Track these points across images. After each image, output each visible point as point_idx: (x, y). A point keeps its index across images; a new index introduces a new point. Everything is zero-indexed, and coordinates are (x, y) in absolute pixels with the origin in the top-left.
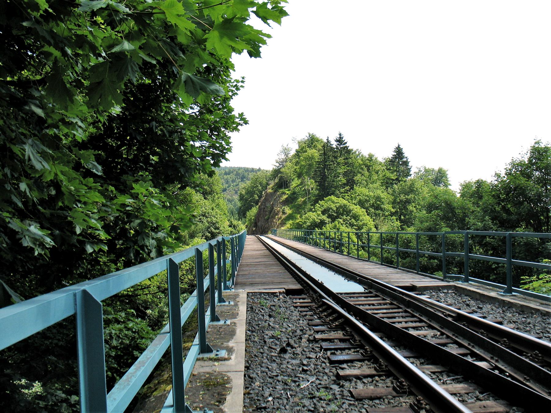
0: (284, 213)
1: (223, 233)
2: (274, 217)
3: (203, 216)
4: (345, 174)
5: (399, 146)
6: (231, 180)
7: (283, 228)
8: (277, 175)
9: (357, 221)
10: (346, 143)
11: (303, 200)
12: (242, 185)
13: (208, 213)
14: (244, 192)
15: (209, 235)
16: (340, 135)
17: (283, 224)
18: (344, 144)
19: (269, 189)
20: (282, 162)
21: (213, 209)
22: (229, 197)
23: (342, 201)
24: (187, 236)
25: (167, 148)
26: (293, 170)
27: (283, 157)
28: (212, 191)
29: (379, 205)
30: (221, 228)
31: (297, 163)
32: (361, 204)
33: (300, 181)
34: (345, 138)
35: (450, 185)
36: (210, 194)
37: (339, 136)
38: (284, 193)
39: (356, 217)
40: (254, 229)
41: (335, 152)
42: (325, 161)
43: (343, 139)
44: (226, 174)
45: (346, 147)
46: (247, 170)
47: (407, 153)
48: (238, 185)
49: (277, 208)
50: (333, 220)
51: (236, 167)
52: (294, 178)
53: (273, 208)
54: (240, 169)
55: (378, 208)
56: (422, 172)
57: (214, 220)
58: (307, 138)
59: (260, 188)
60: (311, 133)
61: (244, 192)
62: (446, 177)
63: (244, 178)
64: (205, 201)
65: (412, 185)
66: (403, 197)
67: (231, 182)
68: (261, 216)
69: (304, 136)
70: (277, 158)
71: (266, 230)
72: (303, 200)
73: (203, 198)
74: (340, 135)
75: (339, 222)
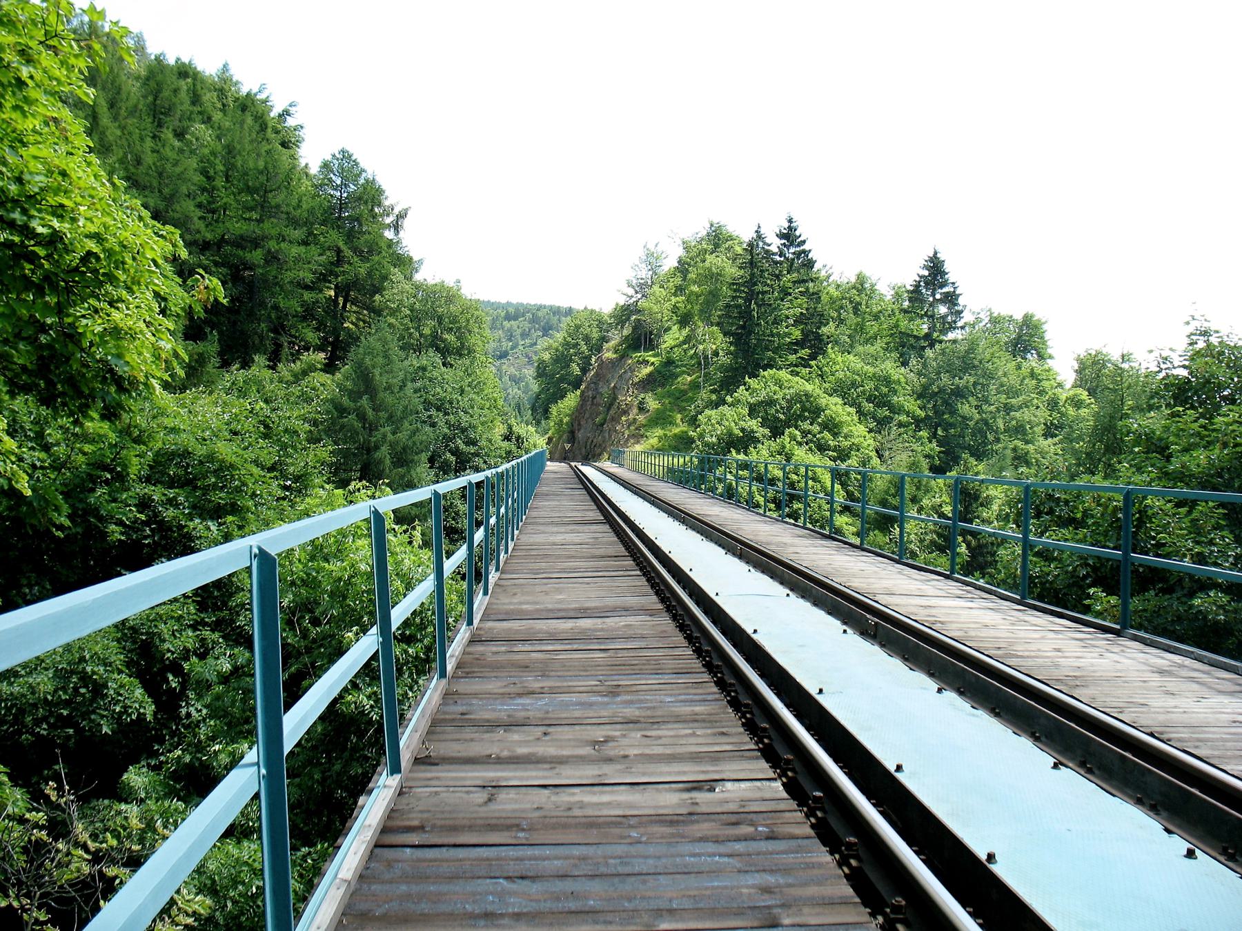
0: (642, 409)
2: (616, 420)
3: (438, 409)
5: (936, 253)
6: (519, 331)
7: (638, 448)
8: (628, 319)
9: (835, 435)
10: (804, 242)
11: (689, 379)
12: (543, 343)
13: (451, 403)
14: (546, 356)
15: (453, 459)
16: (790, 221)
17: (638, 437)
18: (799, 245)
19: (608, 350)
21: (462, 392)
22: (512, 370)
23: (800, 384)
24: (388, 462)
27: (645, 273)
30: (483, 443)
31: (679, 290)
32: (842, 390)
33: (686, 332)
34: (802, 231)
35: (1051, 357)
37: (786, 225)
38: (646, 362)
39: (832, 427)
40: (568, 446)
41: (776, 263)
42: (751, 282)
43: (797, 233)
44: (508, 317)
45: (804, 252)
46: (556, 311)
47: (954, 272)
48: (535, 344)
49: (627, 398)
50: (776, 432)
51: (533, 303)
53: (615, 398)
54: (540, 308)
55: (880, 401)
56: (984, 323)
57: (465, 419)
59: (584, 348)
60: (715, 221)
61: (546, 356)
62: (1042, 338)
63: (551, 328)
65: (972, 346)
66: (945, 379)
68: (587, 415)
69: (697, 229)
70: (630, 275)
71: (598, 451)
72: (689, 379)
74: (790, 221)
75: (793, 438)
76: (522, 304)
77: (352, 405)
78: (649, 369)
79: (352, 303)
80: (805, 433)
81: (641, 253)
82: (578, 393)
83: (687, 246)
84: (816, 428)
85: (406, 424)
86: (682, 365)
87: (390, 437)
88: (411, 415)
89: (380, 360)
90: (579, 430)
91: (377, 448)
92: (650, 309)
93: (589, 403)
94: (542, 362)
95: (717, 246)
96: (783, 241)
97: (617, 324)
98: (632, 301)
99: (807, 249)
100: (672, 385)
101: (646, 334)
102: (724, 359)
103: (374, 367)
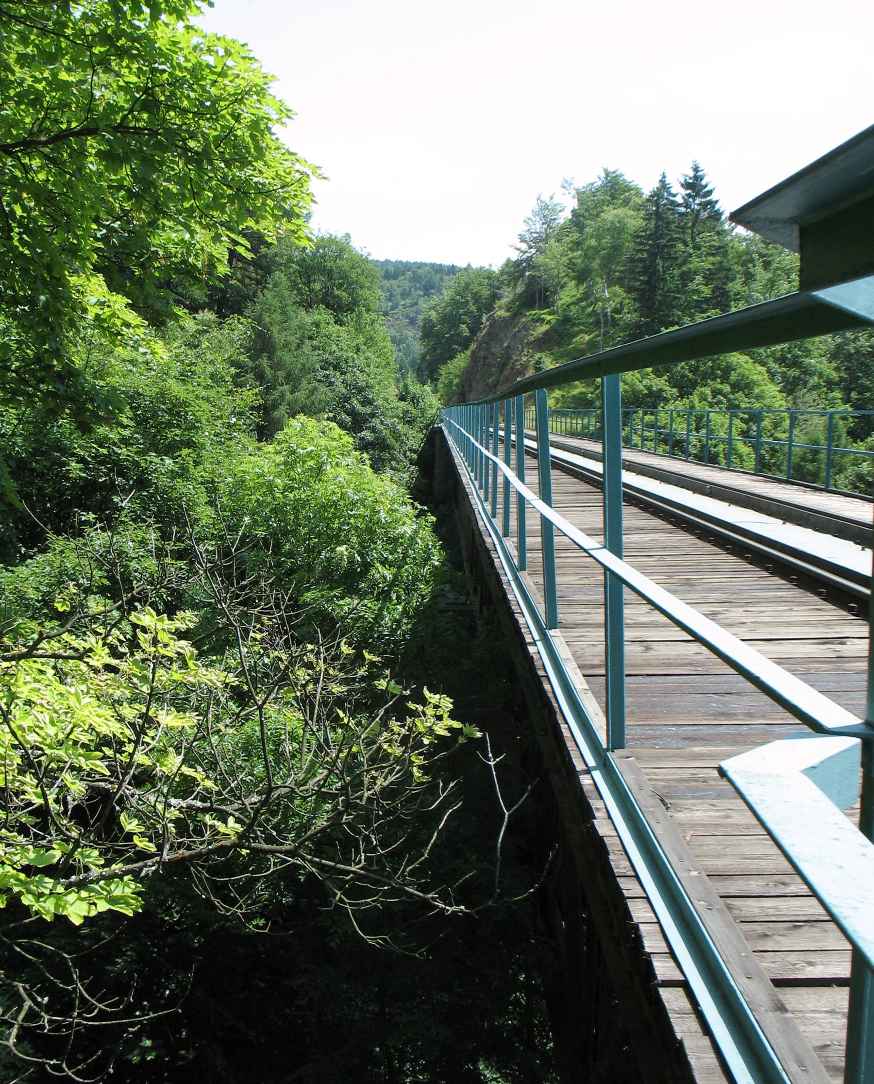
1: (383, 414)
3: (336, 367)
4: (709, 277)
10: (710, 192)
11: (587, 338)
12: (423, 305)
13: (347, 362)
14: (433, 315)
16: (696, 169)
19: (500, 308)
20: (536, 240)
21: (358, 350)
26: (565, 259)
27: (538, 227)
29: (796, 357)
30: (380, 402)
34: (710, 180)
37: (692, 174)
42: (656, 235)
43: (704, 183)
44: (388, 276)
46: (438, 269)
51: (412, 262)
52: (565, 283)
54: (420, 265)
57: (361, 379)
58: (599, 183)
59: (473, 308)
60: (611, 170)
63: (432, 287)
67: (399, 297)
68: (478, 377)
70: (522, 229)
72: (587, 338)
73: (332, 321)
74: (696, 169)
75: (703, 398)
76: (401, 262)
77: (251, 364)
78: (545, 328)
79: (238, 260)
80: (716, 393)
81: (534, 205)
82: (468, 353)
83: (581, 196)
84: (727, 388)
85: (304, 382)
88: (309, 373)
89: (277, 317)
90: (470, 392)
91: (275, 406)
92: (546, 264)
94: (428, 321)
95: (613, 197)
96: (688, 192)
97: (510, 281)
98: (525, 257)
99: (714, 199)
102: (629, 317)
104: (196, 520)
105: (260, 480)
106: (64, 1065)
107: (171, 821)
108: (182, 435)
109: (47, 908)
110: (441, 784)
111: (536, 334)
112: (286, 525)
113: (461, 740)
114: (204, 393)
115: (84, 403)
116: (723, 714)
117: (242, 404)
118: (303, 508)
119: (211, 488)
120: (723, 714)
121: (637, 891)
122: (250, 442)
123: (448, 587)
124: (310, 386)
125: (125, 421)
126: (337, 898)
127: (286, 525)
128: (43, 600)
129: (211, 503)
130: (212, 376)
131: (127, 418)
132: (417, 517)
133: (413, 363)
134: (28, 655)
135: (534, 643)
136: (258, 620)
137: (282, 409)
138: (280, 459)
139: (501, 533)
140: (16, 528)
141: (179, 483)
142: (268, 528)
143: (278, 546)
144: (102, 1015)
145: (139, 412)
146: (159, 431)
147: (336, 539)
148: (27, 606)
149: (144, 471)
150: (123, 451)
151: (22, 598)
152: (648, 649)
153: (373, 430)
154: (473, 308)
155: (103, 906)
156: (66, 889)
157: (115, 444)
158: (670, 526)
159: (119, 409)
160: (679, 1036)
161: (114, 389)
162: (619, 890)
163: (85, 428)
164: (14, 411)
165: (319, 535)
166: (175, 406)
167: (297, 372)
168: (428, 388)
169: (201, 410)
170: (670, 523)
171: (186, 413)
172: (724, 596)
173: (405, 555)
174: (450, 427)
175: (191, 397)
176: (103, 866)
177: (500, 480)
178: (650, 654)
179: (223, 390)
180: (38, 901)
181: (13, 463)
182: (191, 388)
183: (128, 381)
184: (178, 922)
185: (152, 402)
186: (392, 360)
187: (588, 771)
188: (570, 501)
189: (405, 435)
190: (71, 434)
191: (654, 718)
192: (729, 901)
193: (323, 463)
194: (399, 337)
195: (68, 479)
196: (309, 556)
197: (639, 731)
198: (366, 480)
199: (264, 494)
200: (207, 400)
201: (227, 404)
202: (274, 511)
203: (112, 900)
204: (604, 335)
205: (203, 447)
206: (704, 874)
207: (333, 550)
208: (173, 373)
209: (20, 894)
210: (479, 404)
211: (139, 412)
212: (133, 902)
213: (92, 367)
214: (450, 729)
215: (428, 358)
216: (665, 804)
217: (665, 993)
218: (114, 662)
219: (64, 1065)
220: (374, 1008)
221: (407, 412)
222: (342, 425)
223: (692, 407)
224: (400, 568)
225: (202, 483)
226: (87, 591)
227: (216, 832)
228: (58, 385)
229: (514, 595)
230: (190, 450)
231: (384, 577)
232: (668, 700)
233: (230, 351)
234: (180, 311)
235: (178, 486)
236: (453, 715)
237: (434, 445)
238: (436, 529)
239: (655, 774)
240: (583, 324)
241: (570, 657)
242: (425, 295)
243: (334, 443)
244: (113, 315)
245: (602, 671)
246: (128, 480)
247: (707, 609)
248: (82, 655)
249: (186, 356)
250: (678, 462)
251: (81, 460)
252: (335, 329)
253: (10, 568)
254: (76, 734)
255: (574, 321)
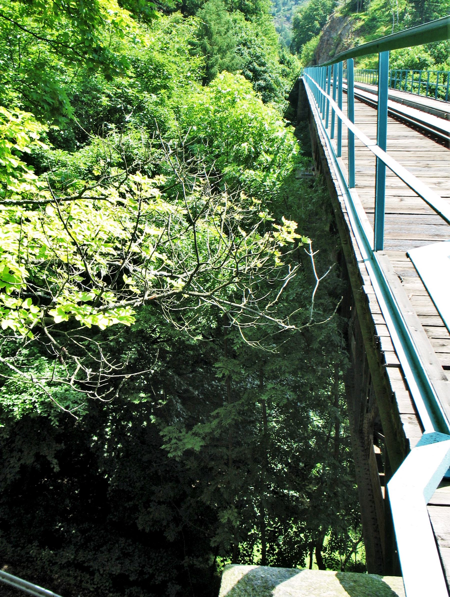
3: (244, 45)
12: (295, 9)
13: (250, 41)
14: (300, 16)
19: (337, 12)
21: (257, 35)
25: (324, 350)
28: (256, 8)
36: (253, 13)
38: (359, 19)
48: (291, 9)
53: (341, 40)
57: (259, 51)
59: (321, 12)
61: (300, 16)
64: (246, 22)
67: (281, 5)
68: (324, 51)
73: (243, 19)
78: (362, 23)
82: (319, 37)
85: (228, 53)
86: (381, 21)
87: (220, 61)
89: (214, 17)
90: (319, 59)
91: (212, 66)
93: (325, 43)
94: (296, 19)
100: (374, 33)
101: (360, 2)
103: (211, 20)
104: (169, 128)
105: (202, 107)
106: (96, 394)
107: (150, 280)
108: (161, 82)
109: (88, 322)
110: (290, 267)
111: (356, 27)
112: (216, 131)
113: (300, 244)
114: (173, 59)
115: (108, 65)
116: (437, 235)
117: (194, 65)
118: (225, 122)
119: (177, 110)
120: (437, 235)
121: (381, 321)
122: (198, 86)
123: (301, 165)
124: (232, 56)
125: (130, 74)
126: (234, 322)
127: (216, 131)
128: (89, 170)
129: (177, 119)
130: (178, 50)
131: (132, 72)
132: (286, 127)
133: (288, 43)
134: (79, 197)
135: (342, 195)
136: (198, 180)
137: (216, 68)
138: (213, 95)
139: (329, 137)
140: (75, 132)
141: (160, 108)
142: (206, 133)
143: (211, 142)
144: (114, 371)
145: (138, 70)
146: (149, 80)
147: (240, 139)
148: (80, 173)
149: (141, 102)
150: (130, 91)
151: (77, 168)
152: (401, 200)
153: (265, 80)
154: (321, 12)
155: (116, 321)
156: (98, 312)
157: (126, 87)
158: (422, 135)
159: (127, 68)
160: (393, 390)
161: (124, 57)
162: (372, 320)
163: (109, 78)
164: (72, 69)
165: (233, 137)
166: (157, 66)
167: (225, 47)
168: (296, 57)
169: (171, 69)
170: (422, 134)
171: (164, 70)
172: (446, 174)
173: (278, 148)
174: (307, 78)
175: (166, 61)
176: (116, 302)
177: (330, 109)
178: (403, 203)
179: (184, 58)
180: (84, 318)
181: (72, 98)
182: (166, 57)
183: (133, 53)
184: (159, 337)
185: (145, 64)
186: (277, 42)
187: (363, 261)
188: (369, 121)
189: (282, 83)
190: (102, 82)
191: (401, 236)
192: (427, 328)
193: (235, 98)
194: (281, 28)
195: (101, 106)
196: (227, 148)
197: (392, 242)
198: (257, 107)
199: (204, 115)
200: (175, 63)
201: (186, 65)
202: (209, 123)
203: (121, 319)
204: (394, 28)
205: (173, 89)
206: (416, 315)
207: (240, 145)
208: (157, 48)
209: (75, 314)
210: (321, 66)
211: (138, 70)
212: (130, 319)
213: (113, 45)
214: (295, 239)
215: (296, 40)
216: (401, 279)
217: (389, 370)
218: (121, 200)
219: (96, 394)
220: (257, 382)
221: (284, 70)
222: (247, 77)
223: (443, 69)
224: (276, 155)
225: (172, 108)
226: (110, 165)
227: (172, 286)
228: (94, 55)
229: (333, 170)
230: (166, 90)
231: (267, 160)
232: (409, 227)
233: (188, 37)
234: (159, 14)
235: (159, 110)
236: (296, 231)
237: (298, 89)
238: (296, 134)
239: (398, 264)
240: (383, 21)
241: (360, 203)
242: (295, 4)
243: (241, 87)
244: (122, 21)
245: (373, 211)
246: (133, 107)
247: (436, 180)
248: (105, 198)
249: (164, 39)
250: (430, 100)
251: (108, 96)
252: (244, 23)
253: (71, 153)
254: (101, 235)
255: (378, 19)
